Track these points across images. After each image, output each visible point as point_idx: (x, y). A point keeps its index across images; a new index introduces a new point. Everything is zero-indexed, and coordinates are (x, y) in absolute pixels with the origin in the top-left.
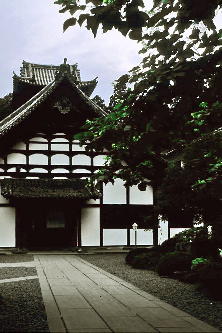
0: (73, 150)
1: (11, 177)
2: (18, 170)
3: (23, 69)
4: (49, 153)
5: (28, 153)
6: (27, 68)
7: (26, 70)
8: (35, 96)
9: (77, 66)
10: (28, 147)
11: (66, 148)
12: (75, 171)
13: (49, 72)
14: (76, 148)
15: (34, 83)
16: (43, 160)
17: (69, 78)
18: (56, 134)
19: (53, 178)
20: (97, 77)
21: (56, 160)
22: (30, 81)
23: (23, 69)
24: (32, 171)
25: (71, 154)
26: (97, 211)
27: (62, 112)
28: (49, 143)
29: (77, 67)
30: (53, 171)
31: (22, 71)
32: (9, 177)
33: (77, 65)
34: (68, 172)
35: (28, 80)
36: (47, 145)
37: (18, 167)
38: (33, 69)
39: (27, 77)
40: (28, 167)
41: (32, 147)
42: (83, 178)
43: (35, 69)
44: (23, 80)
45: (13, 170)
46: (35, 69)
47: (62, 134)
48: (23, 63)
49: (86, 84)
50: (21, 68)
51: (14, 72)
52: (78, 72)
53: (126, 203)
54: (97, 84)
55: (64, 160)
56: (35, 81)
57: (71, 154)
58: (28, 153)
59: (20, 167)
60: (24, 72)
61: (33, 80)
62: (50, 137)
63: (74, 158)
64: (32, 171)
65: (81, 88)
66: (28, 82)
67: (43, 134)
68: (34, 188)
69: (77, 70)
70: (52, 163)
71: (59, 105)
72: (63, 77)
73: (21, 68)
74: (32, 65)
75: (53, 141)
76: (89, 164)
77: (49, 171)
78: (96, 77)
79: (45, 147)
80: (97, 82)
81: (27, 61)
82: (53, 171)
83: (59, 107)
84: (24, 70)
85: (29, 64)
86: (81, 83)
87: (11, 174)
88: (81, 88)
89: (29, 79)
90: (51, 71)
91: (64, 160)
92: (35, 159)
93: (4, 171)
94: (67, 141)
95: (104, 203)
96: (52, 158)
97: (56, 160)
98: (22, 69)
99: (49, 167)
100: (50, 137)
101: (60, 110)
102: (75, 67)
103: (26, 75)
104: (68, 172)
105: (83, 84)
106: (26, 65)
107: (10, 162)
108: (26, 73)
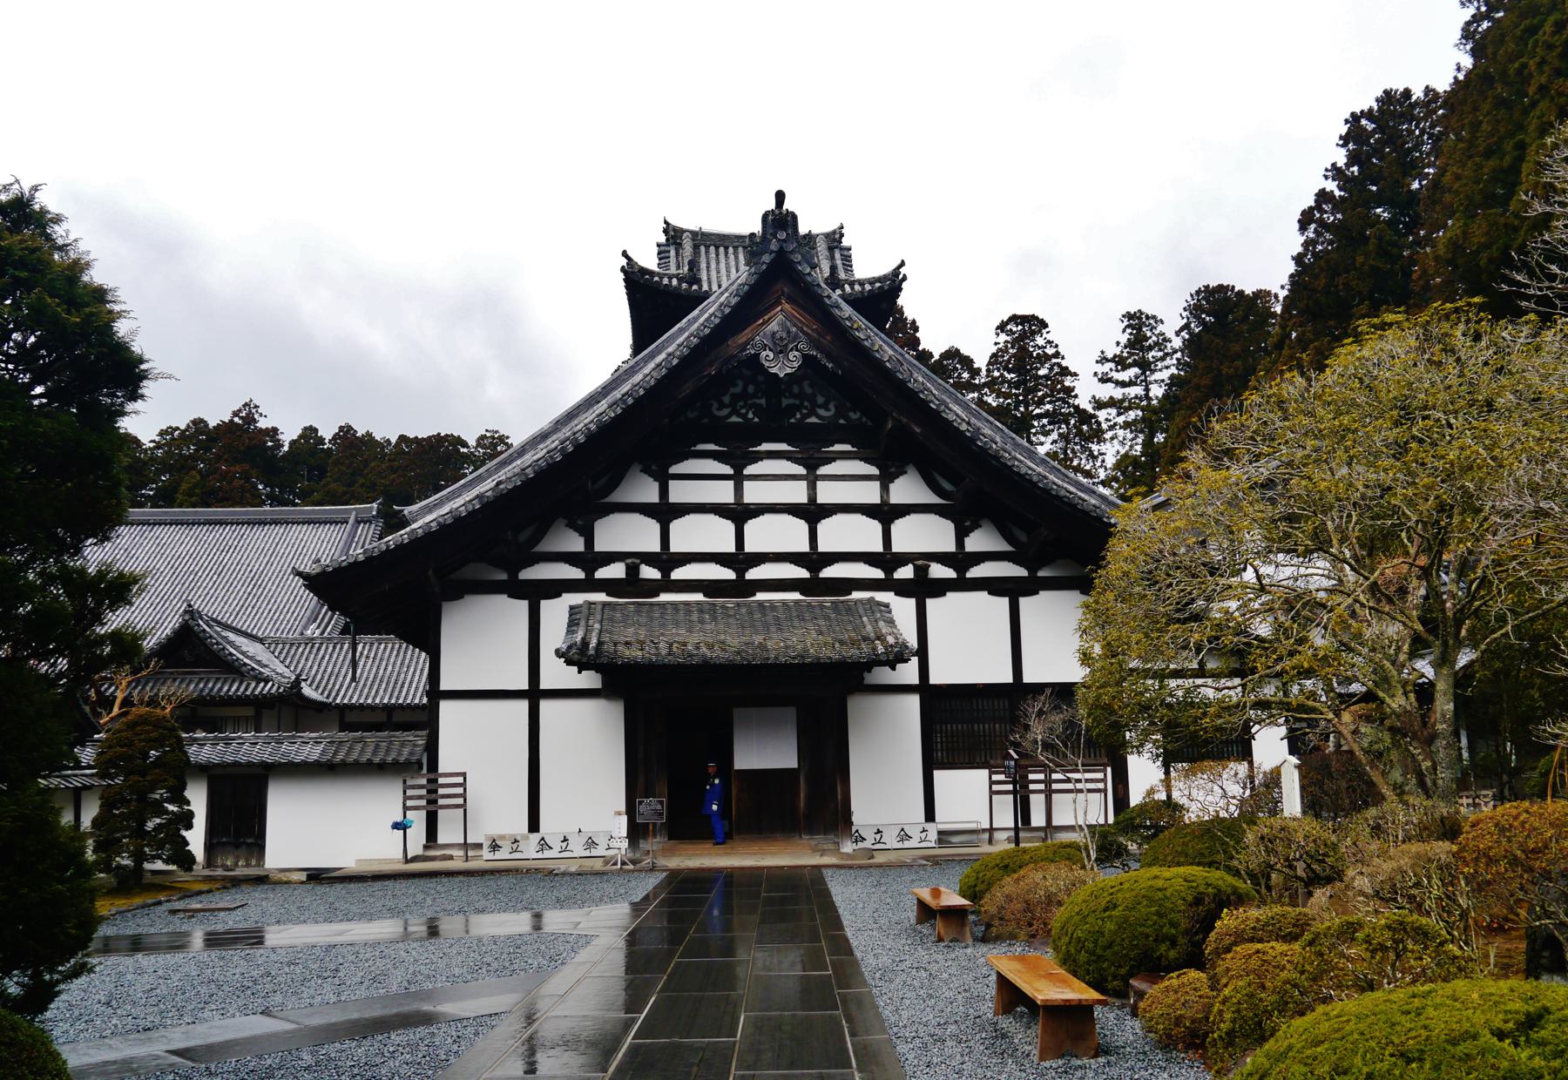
0: (822, 499)
2: (632, 571)
3: (667, 249)
5: (665, 513)
6: (679, 246)
7: (673, 253)
8: (685, 320)
9: (842, 235)
10: (664, 492)
11: (797, 493)
12: (830, 572)
15: (695, 287)
16: (716, 535)
17: (792, 257)
18: (759, 448)
19: (754, 595)
20: (903, 261)
21: (764, 534)
22: (680, 280)
23: (667, 249)
24: (678, 574)
26: (913, 702)
27: (773, 371)
28: (738, 479)
29: (843, 240)
30: (753, 574)
31: (663, 255)
32: (601, 597)
33: (843, 231)
34: (803, 573)
38: (696, 248)
41: (680, 492)
42: (856, 595)
43: (703, 249)
44: (656, 279)
45: (616, 571)
46: (703, 249)
47: (783, 447)
48: (665, 231)
50: (659, 245)
51: (625, 254)
52: (846, 253)
53: (1010, 679)
54: (904, 285)
55: (788, 534)
56: (698, 281)
57: (886, 514)
58: (665, 513)
59: (638, 561)
60: (669, 257)
62: (739, 458)
63: (825, 527)
64: (678, 574)
65: (853, 301)
66: (675, 282)
67: (717, 448)
68: (683, 632)
69: (842, 249)
72: (772, 252)
73: (659, 245)
74: (694, 234)
75: (750, 470)
76: (730, 547)
77: (741, 573)
78: (899, 262)
79: (723, 493)
80: (905, 278)
81: (677, 222)
82: (753, 574)
84: (669, 252)
85: (683, 231)
86: (852, 284)
87: (609, 586)
88: (856, 302)
89: (676, 276)
92: (691, 534)
94: (801, 470)
95: (935, 679)
96: (820, 527)
97: (764, 534)
98: (662, 248)
100: (739, 458)
101: (767, 364)
102: (834, 239)
104: (803, 573)
105: (857, 287)
106: (673, 235)
107: (601, 545)
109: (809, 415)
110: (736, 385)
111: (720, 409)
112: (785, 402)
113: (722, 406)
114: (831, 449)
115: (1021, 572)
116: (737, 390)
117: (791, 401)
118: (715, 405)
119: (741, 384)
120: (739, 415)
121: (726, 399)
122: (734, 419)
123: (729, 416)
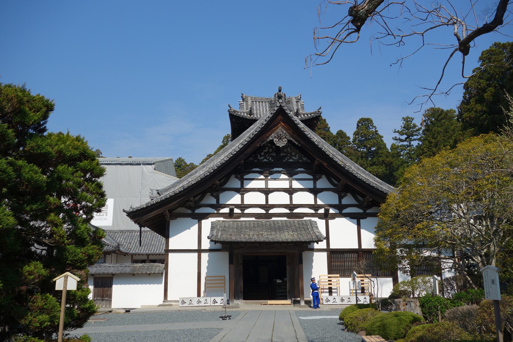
0: (294, 186)
1: (288, 218)
4: (267, 192)
7: (245, 104)
13: (261, 106)
14: (296, 185)
16: (259, 198)
21: (275, 198)
24: (247, 211)
25: (291, 191)
32: (222, 219)
35: (245, 113)
36: (312, 182)
37: (231, 207)
39: (245, 111)
40: (243, 207)
44: (239, 113)
49: (309, 115)
55: (283, 198)
57: (291, 191)
61: (251, 113)
63: (295, 196)
64: (247, 211)
67: (259, 170)
70: (294, 202)
71: (275, 137)
75: (245, 177)
77: (267, 211)
83: (275, 140)
87: (223, 215)
90: (262, 105)
91: (283, 198)
93: (265, 212)
99: (267, 207)
103: (245, 108)
105: (306, 115)
108: (245, 106)
109: (290, 159)
110: (265, 149)
111: (260, 157)
112: (282, 154)
113: (261, 156)
114: (297, 170)
115: (361, 211)
116: (266, 151)
117: (284, 154)
118: (259, 156)
119: (267, 149)
120: (267, 159)
121: (263, 154)
122: (265, 160)
123: (264, 159)
